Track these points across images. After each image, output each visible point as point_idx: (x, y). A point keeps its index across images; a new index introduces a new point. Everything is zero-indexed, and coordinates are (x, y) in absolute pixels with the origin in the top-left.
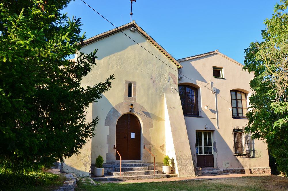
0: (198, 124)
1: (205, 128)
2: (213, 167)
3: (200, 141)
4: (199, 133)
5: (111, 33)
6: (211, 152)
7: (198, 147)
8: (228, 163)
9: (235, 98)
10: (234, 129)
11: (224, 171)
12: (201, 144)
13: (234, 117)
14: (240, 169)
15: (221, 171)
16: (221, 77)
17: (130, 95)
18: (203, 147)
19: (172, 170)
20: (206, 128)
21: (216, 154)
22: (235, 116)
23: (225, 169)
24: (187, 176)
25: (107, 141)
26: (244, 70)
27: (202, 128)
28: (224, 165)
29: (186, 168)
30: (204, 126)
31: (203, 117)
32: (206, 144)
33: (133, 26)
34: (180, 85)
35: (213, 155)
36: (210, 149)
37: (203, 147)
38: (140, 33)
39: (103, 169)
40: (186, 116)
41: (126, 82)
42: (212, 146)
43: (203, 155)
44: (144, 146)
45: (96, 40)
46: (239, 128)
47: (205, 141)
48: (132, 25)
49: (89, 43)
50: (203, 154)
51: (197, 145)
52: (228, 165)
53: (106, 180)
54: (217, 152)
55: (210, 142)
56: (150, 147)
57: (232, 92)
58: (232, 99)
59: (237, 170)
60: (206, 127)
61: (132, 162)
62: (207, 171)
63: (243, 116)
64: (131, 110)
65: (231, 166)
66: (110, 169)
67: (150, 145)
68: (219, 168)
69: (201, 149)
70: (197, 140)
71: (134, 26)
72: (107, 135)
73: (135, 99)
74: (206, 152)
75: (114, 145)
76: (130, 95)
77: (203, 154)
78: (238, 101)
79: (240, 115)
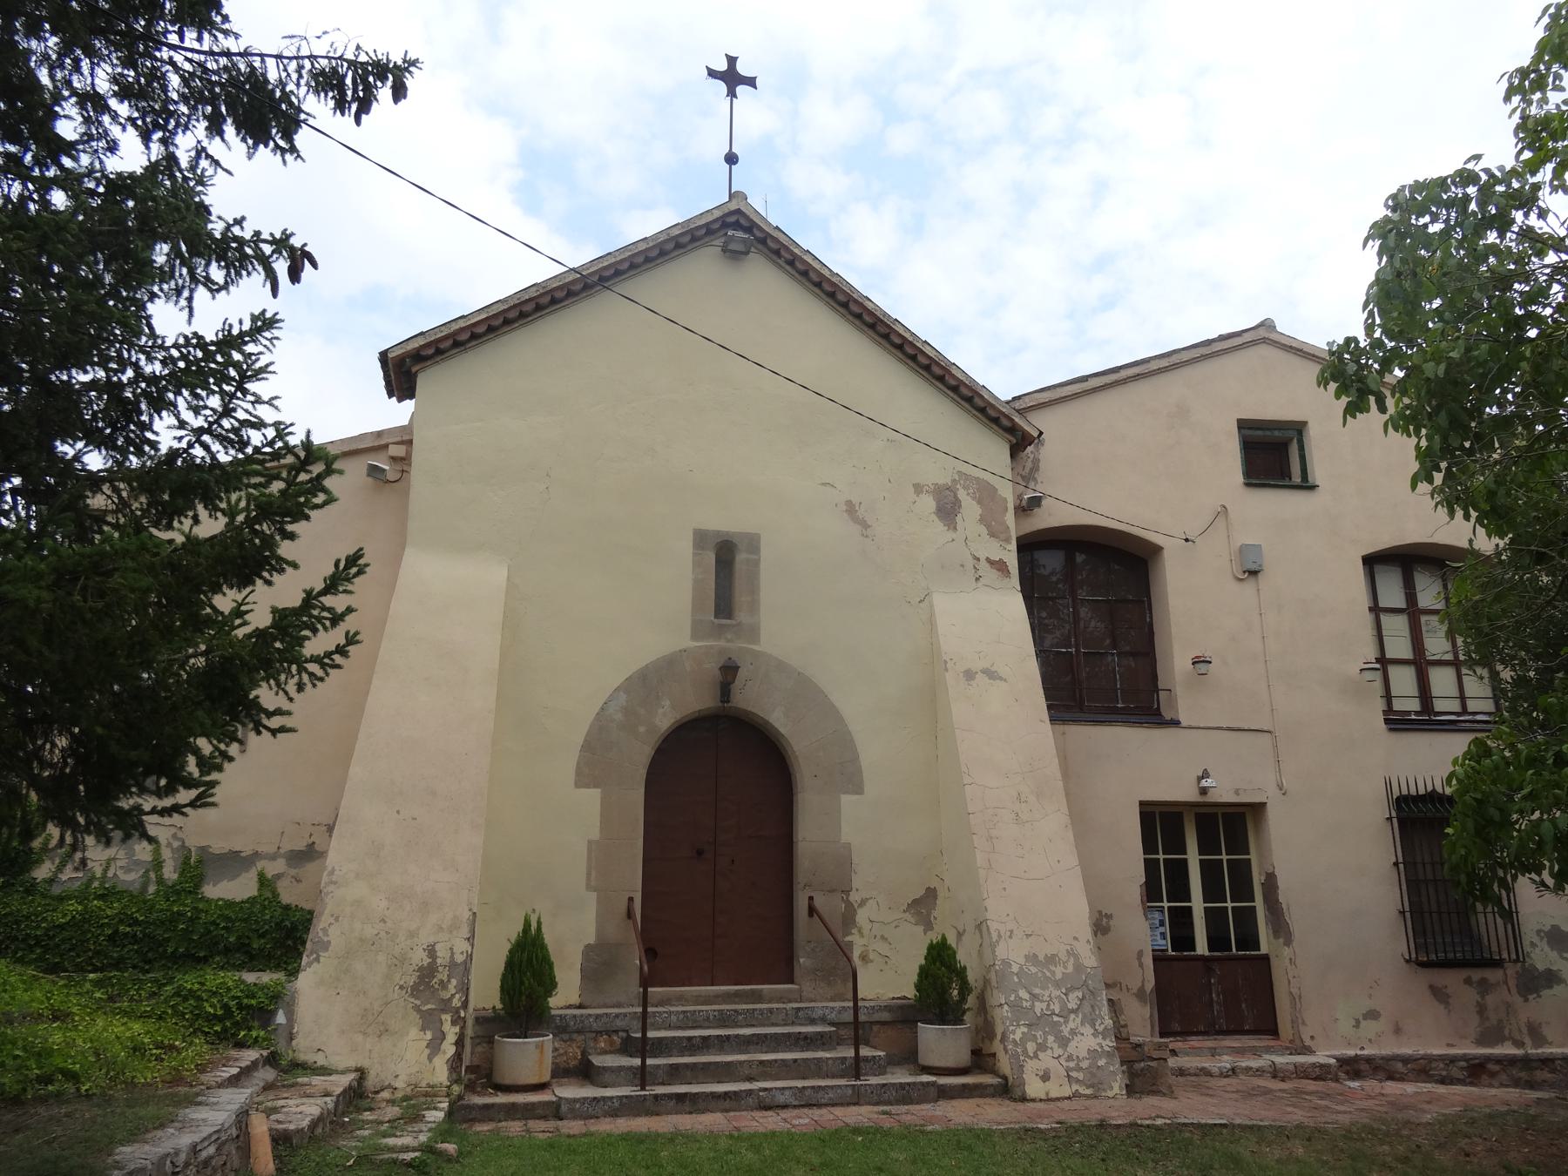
0: (1158, 764)
1: (1197, 791)
2: (1273, 1032)
3: (1178, 872)
4: (1160, 823)
5: (607, 274)
6: (1249, 939)
7: (1166, 904)
8: (1372, 1015)
9: (1400, 603)
10: (1396, 794)
11: (1344, 1062)
12: (1180, 890)
13: (1397, 722)
14: (1464, 1058)
15: (1322, 1066)
16: (1297, 479)
17: (724, 605)
18: (1197, 904)
19: (976, 1053)
20: (1204, 791)
21: (1287, 951)
22: (1409, 713)
23: (1351, 1053)
24: (1067, 1092)
25: (589, 874)
26: (412, 56)
27: (1180, 791)
28: (1345, 1026)
29: (1064, 1042)
30: (1194, 780)
31: (1184, 723)
32: (1212, 891)
33: (737, 226)
34: (1029, 546)
35: (1266, 958)
36: (1246, 918)
37: (1197, 904)
38: (781, 262)
39: (540, 1046)
40: (1064, 721)
41: (701, 538)
42: (1259, 903)
43: (1202, 958)
44: (811, 898)
45: (523, 315)
46: (1413, 792)
47: (1210, 872)
48: (732, 219)
49: (484, 334)
50: (1202, 947)
51: (1151, 892)
52: (1370, 1028)
53: (555, 1111)
54: (1288, 942)
55: (1241, 873)
56: (849, 904)
57: (1377, 568)
58: (1376, 609)
59: (1441, 1058)
60: (1204, 783)
61: (737, 994)
62: (1226, 1062)
63: (1464, 711)
64: (725, 690)
65: (1398, 1030)
66: (595, 1040)
67: (847, 892)
68: (1308, 1042)
69: (1181, 919)
70: (1151, 866)
71: (742, 221)
72: (590, 842)
73: (753, 633)
74: (1217, 941)
75: (631, 899)
76: (724, 605)
77: (1202, 947)
78: (1424, 619)
79: (1439, 706)
